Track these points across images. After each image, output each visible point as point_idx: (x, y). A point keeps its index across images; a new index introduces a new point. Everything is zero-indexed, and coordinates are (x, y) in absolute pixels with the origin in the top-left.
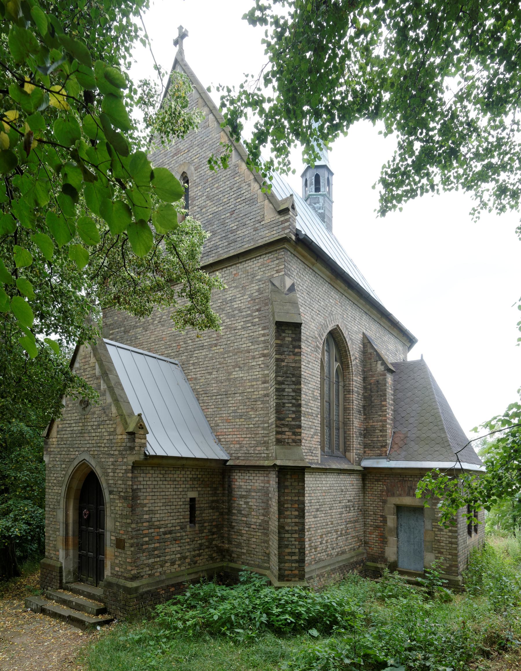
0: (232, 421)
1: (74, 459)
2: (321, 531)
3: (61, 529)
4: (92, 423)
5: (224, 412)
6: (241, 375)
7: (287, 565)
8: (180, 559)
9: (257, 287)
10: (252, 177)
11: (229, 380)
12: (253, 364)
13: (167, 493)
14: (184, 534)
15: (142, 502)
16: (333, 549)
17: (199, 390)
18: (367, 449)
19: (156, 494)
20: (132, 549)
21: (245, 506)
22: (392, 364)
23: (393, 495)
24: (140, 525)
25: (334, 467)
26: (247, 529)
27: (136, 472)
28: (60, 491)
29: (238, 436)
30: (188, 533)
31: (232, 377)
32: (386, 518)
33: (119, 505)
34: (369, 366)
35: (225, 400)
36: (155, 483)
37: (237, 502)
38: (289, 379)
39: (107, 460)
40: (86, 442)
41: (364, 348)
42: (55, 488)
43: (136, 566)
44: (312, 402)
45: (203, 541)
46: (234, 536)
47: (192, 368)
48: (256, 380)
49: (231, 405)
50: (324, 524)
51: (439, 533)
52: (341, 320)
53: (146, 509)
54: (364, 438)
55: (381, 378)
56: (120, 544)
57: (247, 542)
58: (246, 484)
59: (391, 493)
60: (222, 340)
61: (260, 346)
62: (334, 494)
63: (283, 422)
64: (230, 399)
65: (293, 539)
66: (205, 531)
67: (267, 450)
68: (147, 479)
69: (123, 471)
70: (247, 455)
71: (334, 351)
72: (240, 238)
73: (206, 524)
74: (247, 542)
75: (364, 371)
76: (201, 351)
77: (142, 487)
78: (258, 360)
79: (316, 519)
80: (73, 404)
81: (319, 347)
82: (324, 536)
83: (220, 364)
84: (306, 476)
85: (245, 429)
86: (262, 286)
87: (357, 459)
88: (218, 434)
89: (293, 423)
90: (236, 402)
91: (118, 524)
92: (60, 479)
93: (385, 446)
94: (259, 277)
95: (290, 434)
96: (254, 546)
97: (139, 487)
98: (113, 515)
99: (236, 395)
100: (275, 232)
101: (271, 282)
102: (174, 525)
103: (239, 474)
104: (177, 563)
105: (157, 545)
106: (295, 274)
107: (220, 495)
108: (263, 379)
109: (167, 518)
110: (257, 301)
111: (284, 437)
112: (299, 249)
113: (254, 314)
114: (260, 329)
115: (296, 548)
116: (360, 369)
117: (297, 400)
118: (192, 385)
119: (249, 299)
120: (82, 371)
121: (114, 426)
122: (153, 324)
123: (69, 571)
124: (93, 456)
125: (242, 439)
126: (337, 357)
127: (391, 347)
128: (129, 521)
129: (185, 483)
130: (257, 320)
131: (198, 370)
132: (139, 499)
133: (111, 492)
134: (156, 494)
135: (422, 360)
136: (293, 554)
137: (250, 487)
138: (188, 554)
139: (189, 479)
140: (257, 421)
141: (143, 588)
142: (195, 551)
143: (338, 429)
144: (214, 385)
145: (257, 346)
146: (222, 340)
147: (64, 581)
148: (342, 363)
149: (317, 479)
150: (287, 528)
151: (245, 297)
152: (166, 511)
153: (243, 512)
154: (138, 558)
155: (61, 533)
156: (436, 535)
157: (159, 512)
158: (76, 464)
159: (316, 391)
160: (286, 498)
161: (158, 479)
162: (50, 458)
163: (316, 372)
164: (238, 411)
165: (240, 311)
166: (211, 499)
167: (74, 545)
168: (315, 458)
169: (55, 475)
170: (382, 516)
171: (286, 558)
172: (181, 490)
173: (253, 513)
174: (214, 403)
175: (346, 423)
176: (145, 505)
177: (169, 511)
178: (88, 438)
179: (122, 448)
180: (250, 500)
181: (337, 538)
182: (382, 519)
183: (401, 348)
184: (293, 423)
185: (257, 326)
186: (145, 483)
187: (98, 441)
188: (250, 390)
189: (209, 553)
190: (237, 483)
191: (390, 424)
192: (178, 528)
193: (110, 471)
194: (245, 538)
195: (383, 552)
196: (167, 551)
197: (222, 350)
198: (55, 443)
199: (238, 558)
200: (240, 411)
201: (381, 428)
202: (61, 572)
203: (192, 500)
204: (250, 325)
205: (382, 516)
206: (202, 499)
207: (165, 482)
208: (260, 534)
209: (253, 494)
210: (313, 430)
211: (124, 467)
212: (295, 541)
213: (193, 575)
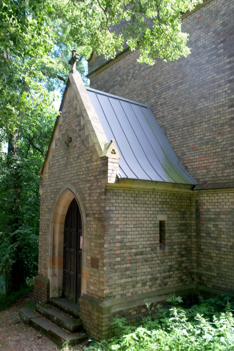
0: (198, 148)
1: (60, 189)
3: (50, 250)
4: (73, 156)
5: (191, 141)
6: (206, 105)
8: (151, 280)
9: (221, 22)
11: (195, 111)
12: (218, 92)
13: (138, 216)
14: (154, 255)
15: (114, 222)
17: (166, 126)
19: (128, 215)
21: (214, 229)
24: (112, 245)
26: (217, 252)
27: (109, 194)
28: (49, 218)
29: (205, 162)
30: (159, 255)
31: (197, 108)
35: (191, 130)
36: (127, 205)
37: (206, 225)
39: (85, 186)
40: (69, 173)
42: (46, 215)
43: (108, 286)
45: (173, 263)
46: (203, 259)
48: (223, 105)
49: (197, 134)
57: (217, 265)
58: (214, 207)
61: (226, 73)
64: (196, 128)
66: (175, 253)
68: (119, 201)
70: (215, 179)
73: (175, 247)
77: (114, 208)
78: (224, 87)
80: (60, 143)
85: (212, 154)
88: (185, 162)
90: (202, 130)
91: (93, 244)
92: (50, 207)
94: (223, 12)
96: (226, 270)
97: (112, 208)
98: (89, 236)
99: (202, 124)
102: (145, 246)
104: (148, 284)
105: (129, 265)
107: (188, 219)
108: (230, 104)
109: (138, 240)
110: (221, 34)
113: (219, 46)
114: (226, 58)
119: (214, 35)
120: (67, 114)
121: (91, 154)
122: (127, 80)
123: (55, 287)
124: (74, 184)
125: (209, 164)
129: (154, 206)
130: (222, 51)
131: (166, 108)
132: (112, 220)
133: (87, 215)
134: (128, 215)
137: (218, 210)
138: (158, 275)
139: (158, 203)
140: (225, 145)
141: (115, 308)
142: (165, 272)
144: (180, 119)
145: (222, 75)
147: (51, 296)
152: (137, 233)
153: (212, 235)
154: (111, 278)
155: (50, 253)
157: (130, 233)
161: (130, 202)
162: (43, 190)
164: (204, 138)
166: (179, 222)
167: (59, 264)
169: (47, 204)
172: (151, 212)
173: (223, 236)
174: (181, 135)
177: (140, 232)
178: (70, 169)
179: (96, 174)
180: (219, 223)
185: (223, 56)
186: (117, 205)
187: (78, 171)
188: (216, 117)
189: (179, 275)
190: (205, 207)
192: (149, 249)
193: (87, 195)
194: (215, 261)
196: (138, 271)
198: (47, 177)
199: (208, 281)
200: (206, 138)
202: (48, 288)
203: (162, 224)
206: (171, 222)
207: (135, 205)
208: (231, 257)
209: (222, 216)
211: (98, 191)
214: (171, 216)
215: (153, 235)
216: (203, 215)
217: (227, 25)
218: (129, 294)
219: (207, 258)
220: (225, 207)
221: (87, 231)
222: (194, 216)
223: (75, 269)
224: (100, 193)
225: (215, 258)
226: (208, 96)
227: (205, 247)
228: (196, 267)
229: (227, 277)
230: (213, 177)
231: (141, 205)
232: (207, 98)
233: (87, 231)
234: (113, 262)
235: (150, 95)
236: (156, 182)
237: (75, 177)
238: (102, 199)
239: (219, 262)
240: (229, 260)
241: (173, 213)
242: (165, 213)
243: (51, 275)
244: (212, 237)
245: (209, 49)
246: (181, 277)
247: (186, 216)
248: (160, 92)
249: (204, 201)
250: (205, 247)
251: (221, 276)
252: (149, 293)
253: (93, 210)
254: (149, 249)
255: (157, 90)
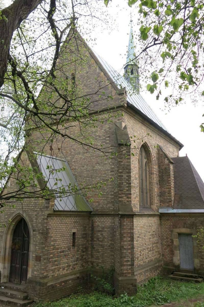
0: (94, 191)
1: (13, 213)
2: (140, 248)
6: (99, 168)
7: (125, 267)
8: (67, 266)
9: (108, 126)
10: (106, 78)
11: (93, 170)
13: (62, 230)
14: (69, 252)
16: (146, 259)
17: (77, 175)
18: (162, 203)
20: (45, 261)
22: (172, 158)
23: (176, 227)
25: (146, 213)
26: (102, 249)
28: (3, 231)
32: (173, 240)
33: (38, 237)
34: (161, 161)
37: (97, 234)
38: (125, 171)
41: (158, 152)
43: (46, 271)
44: (134, 180)
46: (94, 253)
47: (73, 163)
48: (107, 170)
50: (142, 245)
51: (201, 247)
52: (147, 139)
53: (52, 239)
54: (160, 197)
55: (167, 166)
56: (38, 259)
59: (175, 226)
60: (90, 150)
62: (146, 228)
63: (122, 192)
64: (94, 180)
65: (128, 253)
67: (113, 206)
69: (42, 219)
70: (102, 209)
71: (144, 154)
72: (100, 104)
73: (80, 247)
74: (102, 256)
75: (159, 163)
76: (78, 155)
77: (51, 227)
79: (137, 242)
81: (137, 153)
82: (142, 251)
83: (89, 162)
84: (134, 219)
86: (111, 126)
87: (157, 209)
89: (127, 192)
93: (171, 202)
95: (126, 198)
96: (106, 258)
98: (34, 243)
100: (117, 103)
101: (115, 124)
103: (97, 219)
104: (66, 269)
106: (126, 120)
107: (87, 230)
108: (111, 170)
109: (62, 244)
111: (123, 199)
112: (129, 110)
113: (107, 139)
115: (129, 258)
116: (157, 162)
117: (129, 181)
118: (73, 172)
119: (104, 132)
125: (100, 200)
126: (146, 157)
127: (171, 150)
128: (44, 246)
130: (108, 141)
131: (77, 164)
132: (49, 234)
133: (34, 231)
135: (187, 157)
136: (128, 261)
137: (104, 226)
138: (71, 264)
139: (73, 222)
141: (49, 283)
142: (74, 262)
143: (147, 193)
144: (85, 172)
146: (90, 150)
148: (148, 159)
149: (138, 220)
150: (125, 247)
151: (102, 131)
152: (61, 240)
153: (100, 240)
156: (199, 249)
157: (58, 240)
158: (14, 215)
159: (137, 175)
160: (124, 231)
163: (137, 166)
165: (100, 137)
166: (83, 233)
168: (136, 209)
170: (171, 239)
171: (125, 263)
172: (69, 228)
175: (151, 190)
176: (52, 237)
179: (42, 207)
180: (104, 233)
181: (148, 252)
182: (171, 241)
183: (175, 150)
184: (127, 192)
185: (108, 145)
186: (52, 225)
187: (28, 203)
188: (104, 175)
189: (81, 263)
191: (173, 190)
192: (67, 249)
193: (34, 219)
195: (172, 260)
197: (90, 155)
201: (168, 192)
203: (74, 234)
204: (104, 144)
205: (171, 239)
208: (109, 251)
209: (105, 229)
210: (135, 195)
211: (42, 217)
212: (129, 254)
213: (73, 275)
214: (79, 229)
215: (69, 241)
216: (95, 228)
217: (110, 129)
218: (56, 275)
219: (97, 253)
220: (107, 224)
221: (33, 240)
222: (91, 229)
223: (21, 263)
224: (43, 218)
225: (101, 252)
226: (100, 163)
227: (96, 246)
228: (90, 258)
229: (107, 262)
230: (102, 208)
231: (64, 224)
232: (100, 164)
233: (33, 240)
234: (49, 258)
235: (68, 154)
236: (73, 211)
237: (26, 207)
238: (45, 222)
239: (103, 254)
240: (108, 253)
241: (80, 227)
242: (76, 228)
243: (3, 268)
244: (100, 241)
245: (102, 138)
246: (83, 264)
247: (86, 229)
248: (74, 154)
249: (96, 221)
250: (96, 246)
251: (103, 262)
252: (66, 274)
253: (38, 228)
254: (67, 249)
255: (72, 153)
